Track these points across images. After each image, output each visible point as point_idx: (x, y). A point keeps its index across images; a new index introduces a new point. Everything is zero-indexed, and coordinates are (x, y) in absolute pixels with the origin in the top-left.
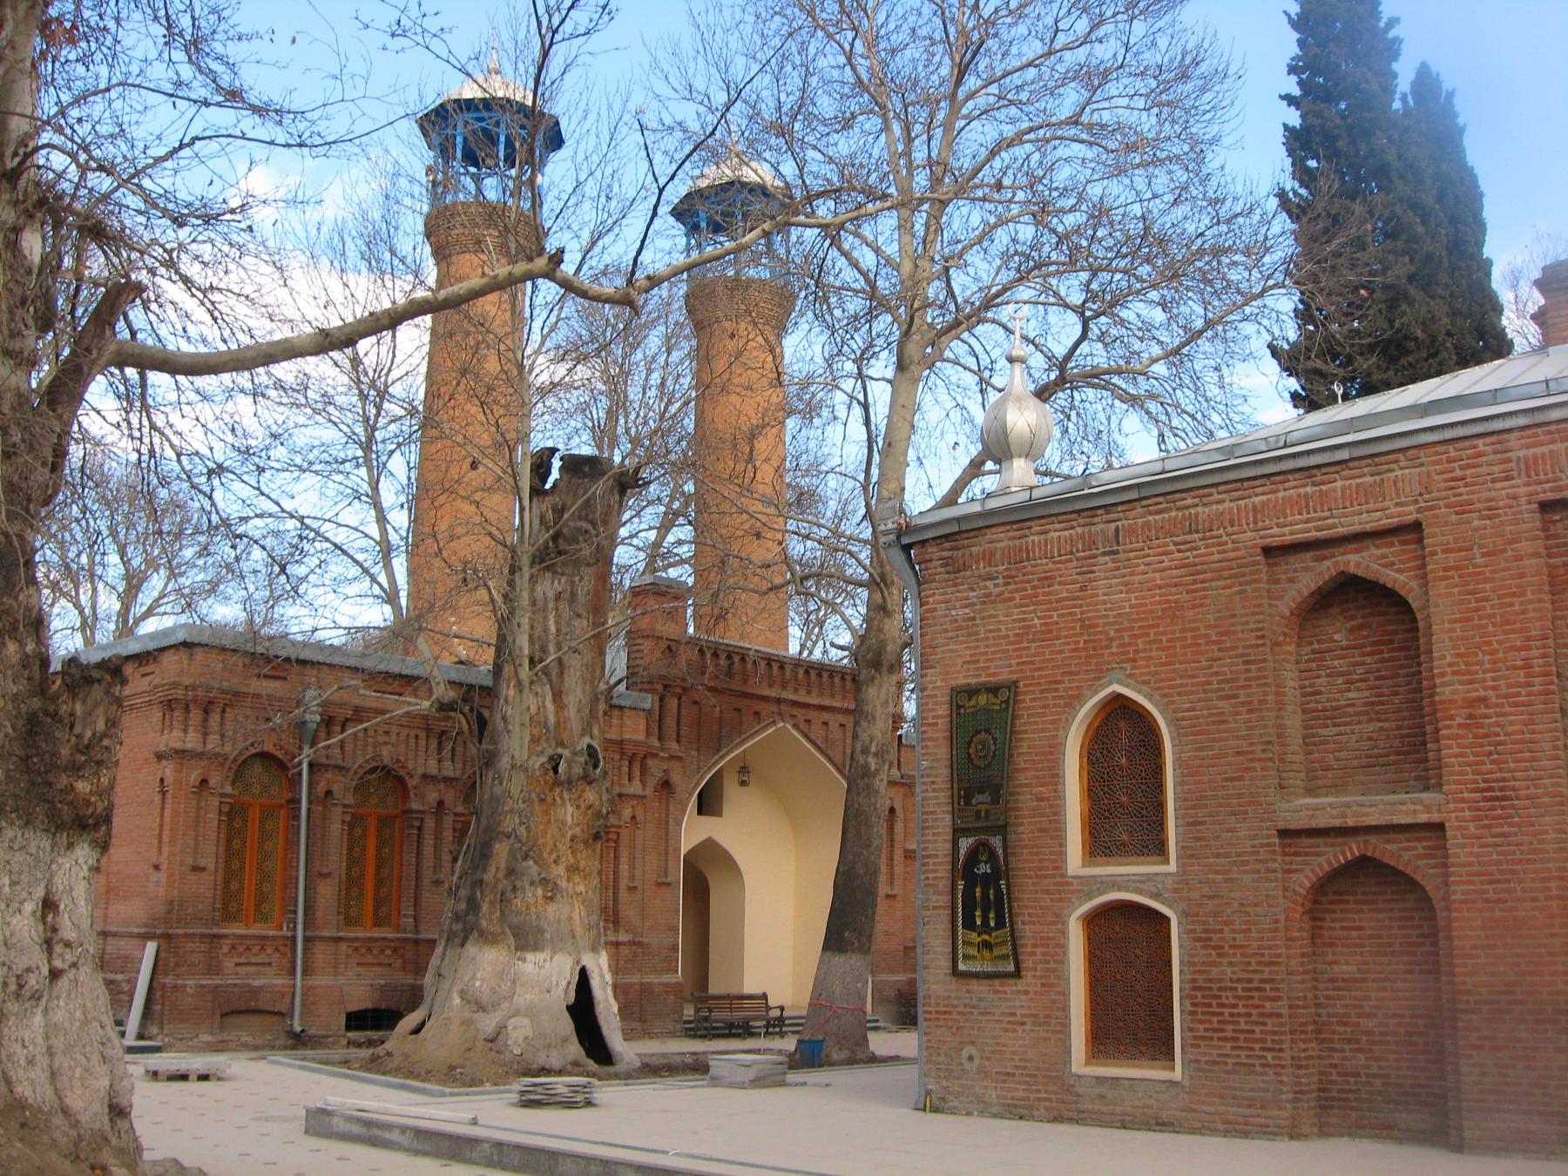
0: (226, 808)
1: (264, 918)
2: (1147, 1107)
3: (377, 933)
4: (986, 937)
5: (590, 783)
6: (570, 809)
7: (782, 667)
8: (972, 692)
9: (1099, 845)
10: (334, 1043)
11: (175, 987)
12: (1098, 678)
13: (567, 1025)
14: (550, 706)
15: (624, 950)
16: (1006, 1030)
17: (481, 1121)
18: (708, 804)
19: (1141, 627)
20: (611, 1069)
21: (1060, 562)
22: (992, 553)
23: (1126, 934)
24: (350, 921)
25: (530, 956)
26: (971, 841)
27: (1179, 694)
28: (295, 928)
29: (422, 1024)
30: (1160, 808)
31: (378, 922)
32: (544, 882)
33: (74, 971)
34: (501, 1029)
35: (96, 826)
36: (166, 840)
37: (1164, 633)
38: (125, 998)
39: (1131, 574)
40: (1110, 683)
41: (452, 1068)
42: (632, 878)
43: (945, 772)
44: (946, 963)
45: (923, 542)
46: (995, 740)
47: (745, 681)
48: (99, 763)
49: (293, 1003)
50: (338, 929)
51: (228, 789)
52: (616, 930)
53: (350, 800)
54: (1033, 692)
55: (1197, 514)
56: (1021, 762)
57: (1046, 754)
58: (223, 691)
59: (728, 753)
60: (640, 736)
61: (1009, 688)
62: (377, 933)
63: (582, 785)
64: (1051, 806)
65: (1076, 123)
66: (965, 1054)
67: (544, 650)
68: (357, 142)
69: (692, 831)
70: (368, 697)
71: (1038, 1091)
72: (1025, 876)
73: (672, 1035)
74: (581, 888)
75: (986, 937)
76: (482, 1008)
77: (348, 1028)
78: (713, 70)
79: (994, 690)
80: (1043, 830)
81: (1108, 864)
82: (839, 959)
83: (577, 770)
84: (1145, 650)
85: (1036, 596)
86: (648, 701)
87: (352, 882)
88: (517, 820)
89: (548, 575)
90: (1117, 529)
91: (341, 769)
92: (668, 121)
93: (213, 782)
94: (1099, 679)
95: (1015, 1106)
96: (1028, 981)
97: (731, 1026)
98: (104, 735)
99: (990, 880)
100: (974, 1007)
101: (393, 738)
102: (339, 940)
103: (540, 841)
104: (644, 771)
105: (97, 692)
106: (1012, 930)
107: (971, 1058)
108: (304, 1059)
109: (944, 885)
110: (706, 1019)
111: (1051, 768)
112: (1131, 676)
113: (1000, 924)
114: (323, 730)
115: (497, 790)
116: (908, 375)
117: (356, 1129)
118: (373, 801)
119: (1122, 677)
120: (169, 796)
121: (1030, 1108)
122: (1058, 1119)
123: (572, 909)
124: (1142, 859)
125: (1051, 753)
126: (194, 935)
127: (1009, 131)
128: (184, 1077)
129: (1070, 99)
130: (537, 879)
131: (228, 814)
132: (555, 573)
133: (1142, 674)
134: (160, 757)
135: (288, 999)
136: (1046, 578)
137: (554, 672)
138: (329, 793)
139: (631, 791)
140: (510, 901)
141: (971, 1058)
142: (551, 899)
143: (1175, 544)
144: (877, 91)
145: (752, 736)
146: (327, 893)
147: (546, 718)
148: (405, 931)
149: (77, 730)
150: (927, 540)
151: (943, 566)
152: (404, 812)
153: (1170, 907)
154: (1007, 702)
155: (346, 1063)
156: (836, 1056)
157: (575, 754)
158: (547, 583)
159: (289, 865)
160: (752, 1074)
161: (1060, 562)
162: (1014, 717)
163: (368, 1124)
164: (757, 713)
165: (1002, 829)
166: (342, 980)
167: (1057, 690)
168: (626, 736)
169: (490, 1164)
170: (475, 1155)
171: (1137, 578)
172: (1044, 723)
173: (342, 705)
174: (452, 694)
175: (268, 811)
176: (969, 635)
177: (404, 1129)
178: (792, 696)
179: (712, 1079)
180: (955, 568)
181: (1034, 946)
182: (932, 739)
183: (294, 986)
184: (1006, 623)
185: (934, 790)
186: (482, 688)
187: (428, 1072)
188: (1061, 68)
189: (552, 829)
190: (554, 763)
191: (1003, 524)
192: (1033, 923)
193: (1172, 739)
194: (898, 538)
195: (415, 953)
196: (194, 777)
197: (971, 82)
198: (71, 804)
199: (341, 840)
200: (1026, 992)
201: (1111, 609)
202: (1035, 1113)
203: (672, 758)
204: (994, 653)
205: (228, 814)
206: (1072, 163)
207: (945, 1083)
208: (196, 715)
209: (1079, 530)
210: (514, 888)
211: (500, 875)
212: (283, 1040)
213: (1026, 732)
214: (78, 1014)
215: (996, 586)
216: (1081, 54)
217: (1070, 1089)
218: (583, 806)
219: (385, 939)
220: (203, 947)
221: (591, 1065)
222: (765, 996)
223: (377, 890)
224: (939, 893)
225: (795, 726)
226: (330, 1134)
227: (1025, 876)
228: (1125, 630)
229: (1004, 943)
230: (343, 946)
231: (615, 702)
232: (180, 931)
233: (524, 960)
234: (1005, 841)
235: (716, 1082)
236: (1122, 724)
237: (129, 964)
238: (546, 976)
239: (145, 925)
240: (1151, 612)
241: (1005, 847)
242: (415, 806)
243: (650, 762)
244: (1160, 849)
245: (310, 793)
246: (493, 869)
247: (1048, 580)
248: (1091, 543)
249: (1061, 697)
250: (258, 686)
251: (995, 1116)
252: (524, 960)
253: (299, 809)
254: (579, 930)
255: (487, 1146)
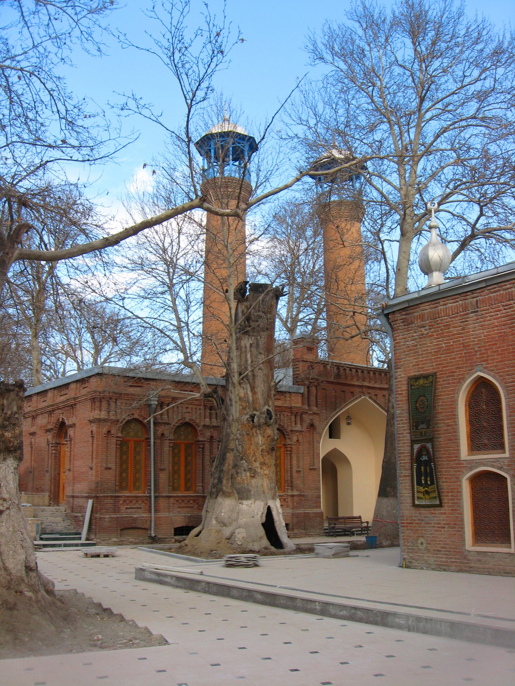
0: (119, 443)
1: (138, 489)
2: (500, 565)
3: (186, 494)
4: (426, 489)
5: (268, 426)
6: (260, 438)
7: (363, 372)
8: (417, 378)
9: (475, 446)
10: (169, 541)
11: (100, 518)
12: (471, 369)
13: (262, 532)
14: (250, 394)
15: (296, 498)
16: (437, 531)
17: (204, 573)
18: (334, 432)
19: (489, 345)
20: (281, 551)
21: (453, 318)
22: (423, 315)
23: (488, 485)
24: (174, 489)
25: (245, 502)
26: (419, 445)
27: (508, 375)
28: (150, 493)
29: (200, 532)
30: (501, 427)
31: (187, 489)
32: (250, 469)
33: (8, 511)
34: (232, 534)
35: (15, 451)
36: (94, 456)
37: (499, 347)
38: (81, 523)
39: (484, 321)
40: (476, 372)
41: (212, 551)
42: (298, 467)
43: (406, 415)
44: (409, 500)
45: (393, 312)
46: (427, 399)
47: (346, 379)
48: (14, 425)
49: (151, 525)
50: (169, 493)
51: (120, 435)
52: (292, 490)
53: (172, 437)
54: (443, 377)
55: (512, 292)
56: (439, 409)
57: (449, 405)
58: (115, 393)
59: (339, 411)
60: (299, 405)
61: (432, 376)
62: (186, 494)
63: (265, 427)
64: (453, 429)
65: (475, 118)
66: (419, 542)
67: (246, 369)
68: (110, 156)
69: (325, 446)
70: (175, 392)
71: (451, 558)
72: (443, 461)
73: (319, 535)
74: (267, 472)
75: (426, 489)
76: (225, 525)
77: (175, 534)
78: (310, 110)
79: (426, 377)
80: (450, 440)
81: (479, 454)
82: (385, 500)
83: (262, 421)
84: (491, 356)
85: (443, 333)
86: (302, 389)
87: (175, 472)
88: (237, 443)
89: (246, 336)
90: (477, 301)
91: (168, 424)
92: (291, 134)
93: (113, 432)
94: (471, 370)
95: (442, 565)
96: (446, 508)
97: (345, 530)
98: (16, 413)
99: (427, 463)
100: (423, 520)
101: (190, 410)
102: (170, 497)
103: (248, 452)
104: (302, 420)
105: (12, 395)
106: (437, 486)
107: (422, 544)
108: (152, 548)
109: (408, 466)
110: (333, 528)
111: (452, 412)
112: (486, 368)
113: (432, 483)
114: (159, 407)
115: (228, 430)
116: (405, 238)
117: (154, 577)
118: (183, 437)
119: (482, 368)
120: (95, 438)
121: (448, 566)
122: (461, 571)
123: (263, 481)
124: (495, 451)
125: (452, 405)
126: (107, 496)
127: (445, 124)
128: (98, 556)
129: (472, 107)
130: (247, 469)
131: (120, 445)
132: (249, 335)
133: (491, 367)
134: (91, 422)
135: (148, 523)
136: (447, 325)
137: (251, 378)
138: (163, 435)
139: (296, 429)
140: (235, 478)
141: (422, 544)
142: (253, 477)
143: (503, 306)
144: (387, 113)
145: (351, 402)
146: (164, 477)
147: (248, 398)
148: (198, 493)
149: (5, 412)
150: (395, 311)
151: (402, 322)
152: (197, 441)
153: (507, 473)
154: (432, 382)
155: (170, 550)
156: (385, 543)
157: (261, 413)
158: (246, 340)
159: (147, 466)
160: (333, 552)
161: (453, 318)
162: (435, 389)
163: (159, 574)
164: (352, 392)
165: (431, 440)
166: (172, 514)
167: (453, 376)
168: (293, 405)
169: (205, 592)
170: (199, 588)
171: (486, 323)
172: (448, 391)
173: (167, 397)
174: (209, 390)
175: (138, 443)
176: (415, 353)
177: (172, 577)
178: (367, 384)
179: (317, 554)
180: (408, 323)
181: (448, 492)
182: (400, 401)
183: (151, 517)
184: (431, 346)
185: (402, 424)
186: (222, 386)
187: (201, 553)
188: (470, 92)
189: (253, 447)
190: (252, 417)
191: (427, 302)
192: (446, 482)
193: (505, 395)
194: (383, 311)
195: (199, 502)
196: (105, 430)
197: (427, 104)
198: (3, 442)
199: (165, 456)
200: (445, 513)
201: (476, 338)
202: (451, 568)
203: (314, 413)
204: (426, 360)
205: (120, 445)
206: (475, 137)
207: (411, 555)
208: (104, 404)
209: (460, 302)
210: (237, 473)
211: (230, 467)
212: (147, 540)
213: (441, 395)
214: (11, 529)
215: (425, 330)
216: (478, 86)
217: (465, 557)
218: (266, 436)
219: (190, 496)
220: (112, 501)
221: (273, 549)
222: (360, 517)
223: (186, 475)
224: (406, 470)
225: (370, 398)
226: (145, 579)
227: (443, 461)
228: (482, 347)
229: (434, 491)
230: (172, 500)
231: (279, 390)
232: (102, 495)
233: (242, 504)
234: (433, 445)
235: (318, 555)
236: (483, 390)
237: (82, 509)
238: (253, 510)
239: (88, 493)
240: (493, 338)
241: (433, 448)
242: (201, 439)
243: (304, 416)
244: (501, 447)
245: (154, 435)
246: (227, 465)
247: (448, 326)
248: (465, 308)
249: (456, 379)
250: (132, 390)
251: (433, 569)
252: (242, 504)
253: (150, 442)
254: (267, 490)
255: (203, 584)
